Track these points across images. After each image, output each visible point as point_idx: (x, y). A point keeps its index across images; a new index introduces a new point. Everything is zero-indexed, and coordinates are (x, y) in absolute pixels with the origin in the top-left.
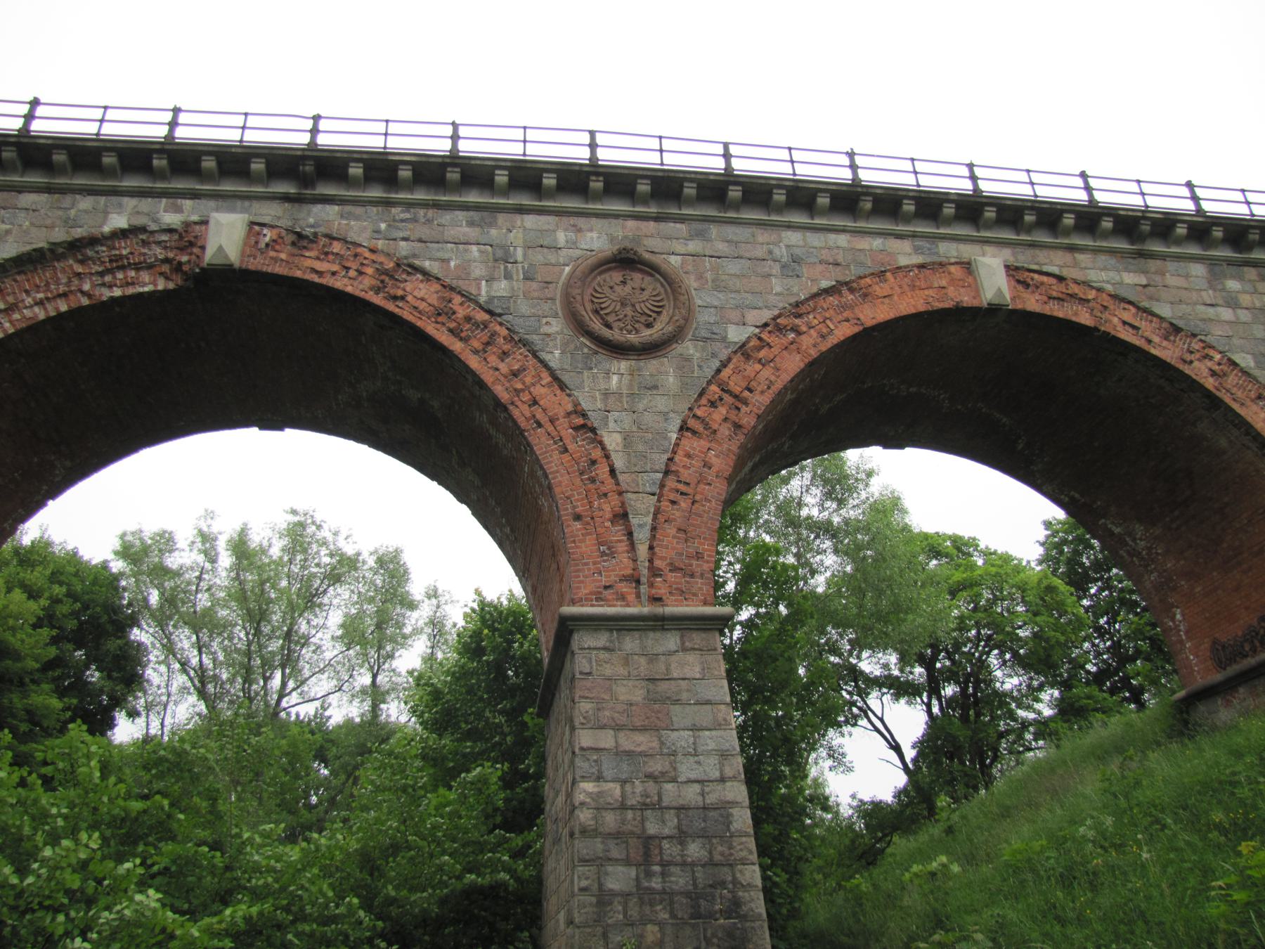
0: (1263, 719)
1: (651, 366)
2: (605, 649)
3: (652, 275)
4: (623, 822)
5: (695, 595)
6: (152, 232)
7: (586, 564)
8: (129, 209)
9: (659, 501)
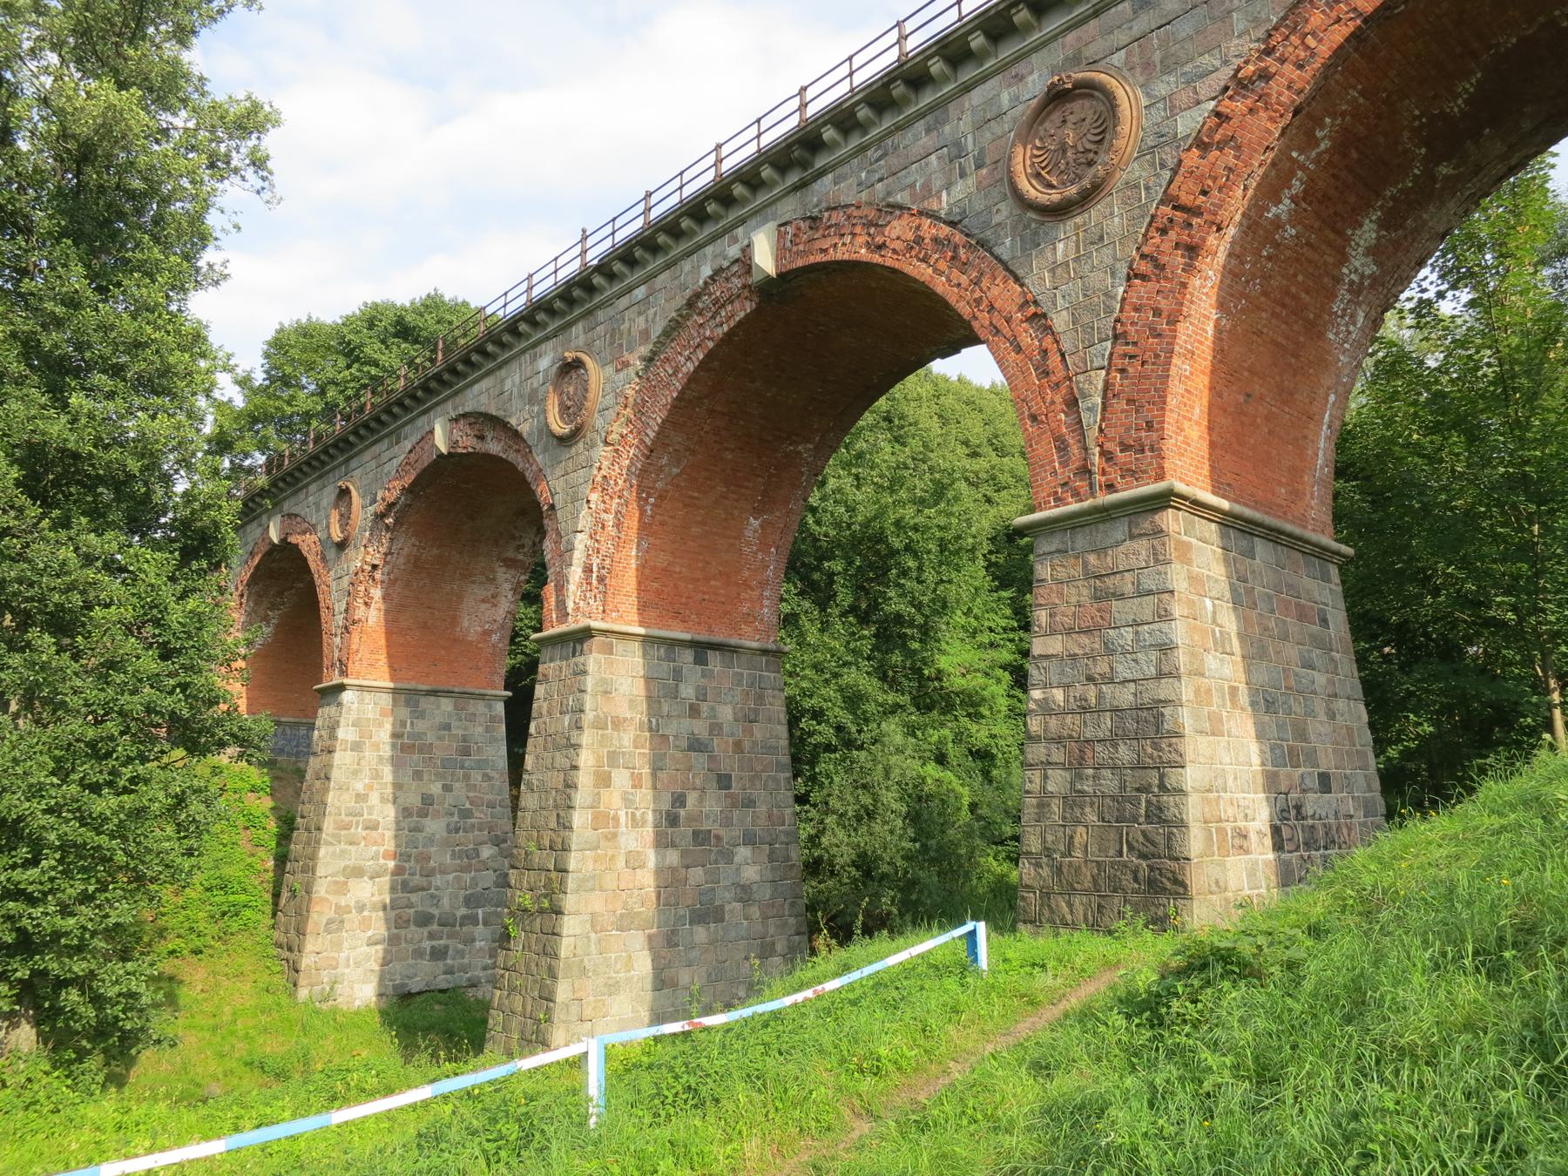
0: (1566, 784)
1: (1094, 213)
2: (1058, 551)
3: (1092, 96)
4: (1063, 726)
5: (1145, 472)
6: (728, 268)
7: (1042, 466)
8: (709, 257)
9: (1108, 374)
